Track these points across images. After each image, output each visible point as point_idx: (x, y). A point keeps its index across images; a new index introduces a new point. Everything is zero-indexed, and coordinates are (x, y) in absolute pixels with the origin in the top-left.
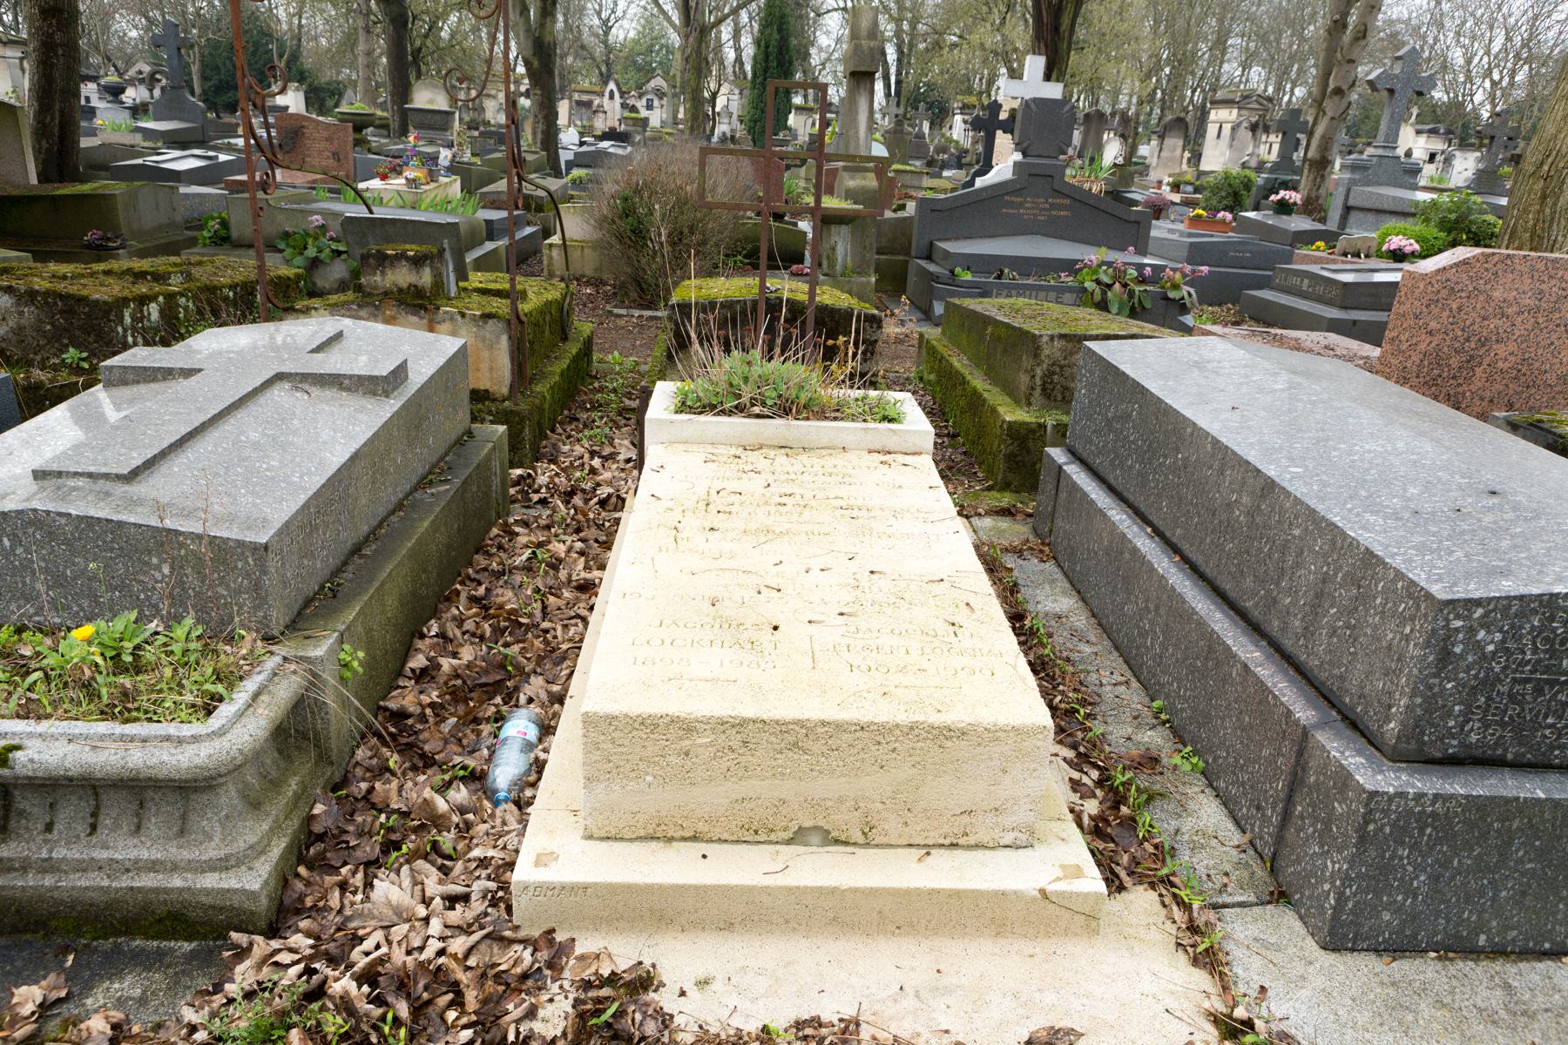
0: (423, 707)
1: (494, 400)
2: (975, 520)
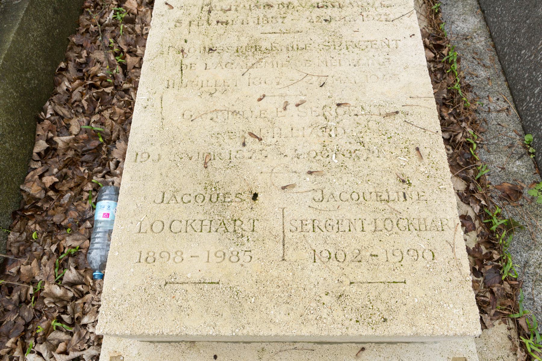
0: (46, 190)
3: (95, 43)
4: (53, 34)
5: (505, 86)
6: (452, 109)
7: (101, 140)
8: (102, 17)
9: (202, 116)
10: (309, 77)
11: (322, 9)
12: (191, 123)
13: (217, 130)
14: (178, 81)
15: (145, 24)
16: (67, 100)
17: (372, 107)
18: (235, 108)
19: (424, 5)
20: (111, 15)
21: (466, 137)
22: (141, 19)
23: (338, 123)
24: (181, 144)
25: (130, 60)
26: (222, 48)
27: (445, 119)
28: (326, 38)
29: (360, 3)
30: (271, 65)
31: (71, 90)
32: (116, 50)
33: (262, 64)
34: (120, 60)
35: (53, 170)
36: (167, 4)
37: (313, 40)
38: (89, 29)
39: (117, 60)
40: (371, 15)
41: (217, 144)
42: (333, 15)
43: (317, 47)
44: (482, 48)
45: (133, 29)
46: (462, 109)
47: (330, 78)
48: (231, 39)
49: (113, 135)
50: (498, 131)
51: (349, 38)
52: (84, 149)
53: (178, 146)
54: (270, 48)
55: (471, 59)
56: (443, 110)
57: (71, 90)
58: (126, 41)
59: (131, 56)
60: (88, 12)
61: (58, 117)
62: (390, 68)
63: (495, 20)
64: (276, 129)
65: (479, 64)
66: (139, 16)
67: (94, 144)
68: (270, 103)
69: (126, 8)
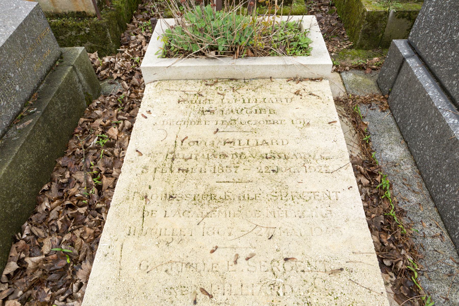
1: (90, 17)
2: (344, 74)
3: (78, 164)
4: (43, 160)
5: (435, 211)
6: (390, 236)
7: (68, 261)
8: (87, 141)
9: (158, 268)
10: (258, 229)
11: (270, 160)
12: (147, 275)
13: (170, 284)
14: (139, 228)
15: (123, 149)
16: (45, 220)
17: (318, 262)
18: (189, 260)
19: (356, 135)
20: (95, 141)
21: (406, 265)
22: (120, 144)
23: (286, 280)
24: (135, 299)
25: (106, 181)
26: (181, 196)
27: (385, 246)
28: (274, 188)
29: (303, 155)
30: (224, 214)
31: (50, 210)
32: (95, 172)
33: (216, 213)
34: (97, 181)
35: (18, 292)
36: (137, 151)
37: (263, 190)
38: (75, 151)
39: (95, 181)
40: (313, 167)
41: (169, 300)
42: (280, 166)
43: (266, 197)
44: (409, 174)
45: (112, 152)
46: (400, 236)
47: (277, 230)
48: (190, 187)
49: (81, 256)
50: (435, 257)
51: (294, 189)
52: (52, 269)
53: (131, 301)
54: (224, 198)
55: (402, 185)
56: (382, 236)
57: (50, 210)
58: (105, 163)
59: (107, 177)
60: (76, 137)
61: (33, 236)
62: (332, 220)
63: (418, 152)
64: (226, 285)
65: (409, 189)
66: (119, 141)
67: (62, 263)
68: (222, 255)
69: (108, 135)
